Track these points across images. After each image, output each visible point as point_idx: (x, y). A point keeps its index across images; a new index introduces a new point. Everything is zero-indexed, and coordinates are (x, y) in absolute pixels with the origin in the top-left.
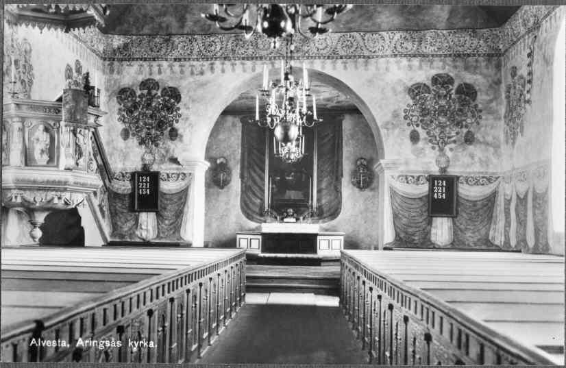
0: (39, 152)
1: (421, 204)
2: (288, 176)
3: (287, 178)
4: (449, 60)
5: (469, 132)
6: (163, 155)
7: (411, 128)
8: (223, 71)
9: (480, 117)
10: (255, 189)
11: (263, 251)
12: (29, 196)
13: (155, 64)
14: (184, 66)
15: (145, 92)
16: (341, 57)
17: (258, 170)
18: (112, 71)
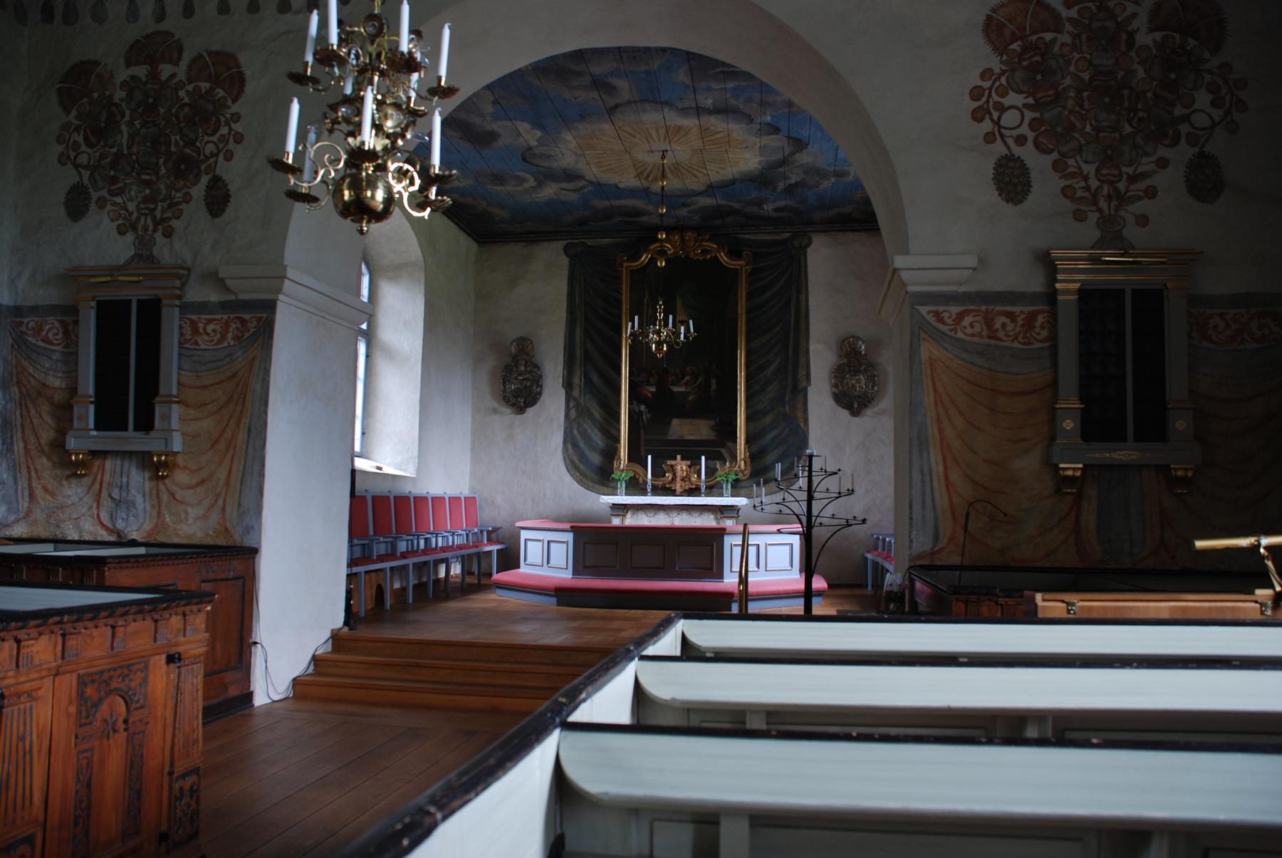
2: (676, 383)
3: (676, 389)
7: (999, 148)
15: (141, 71)
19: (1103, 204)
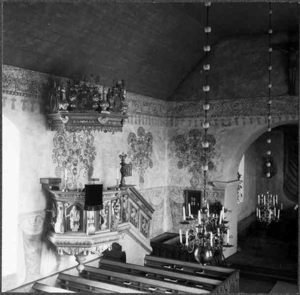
10: (293, 178)
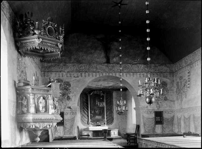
0: (42, 107)
1: (152, 120)
2: (96, 111)
3: (96, 112)
4: (158, 74)
5: (165, 97)
6: (65, 106)
8: (85, 76)
9: (168, 92)
11: (93, 136)
12: (37, 125)
13: (61, 73)
14: (71, 74)
16: (125, 72)
17: (86, 109)
18: (44, 76)
19: (157, 101)
